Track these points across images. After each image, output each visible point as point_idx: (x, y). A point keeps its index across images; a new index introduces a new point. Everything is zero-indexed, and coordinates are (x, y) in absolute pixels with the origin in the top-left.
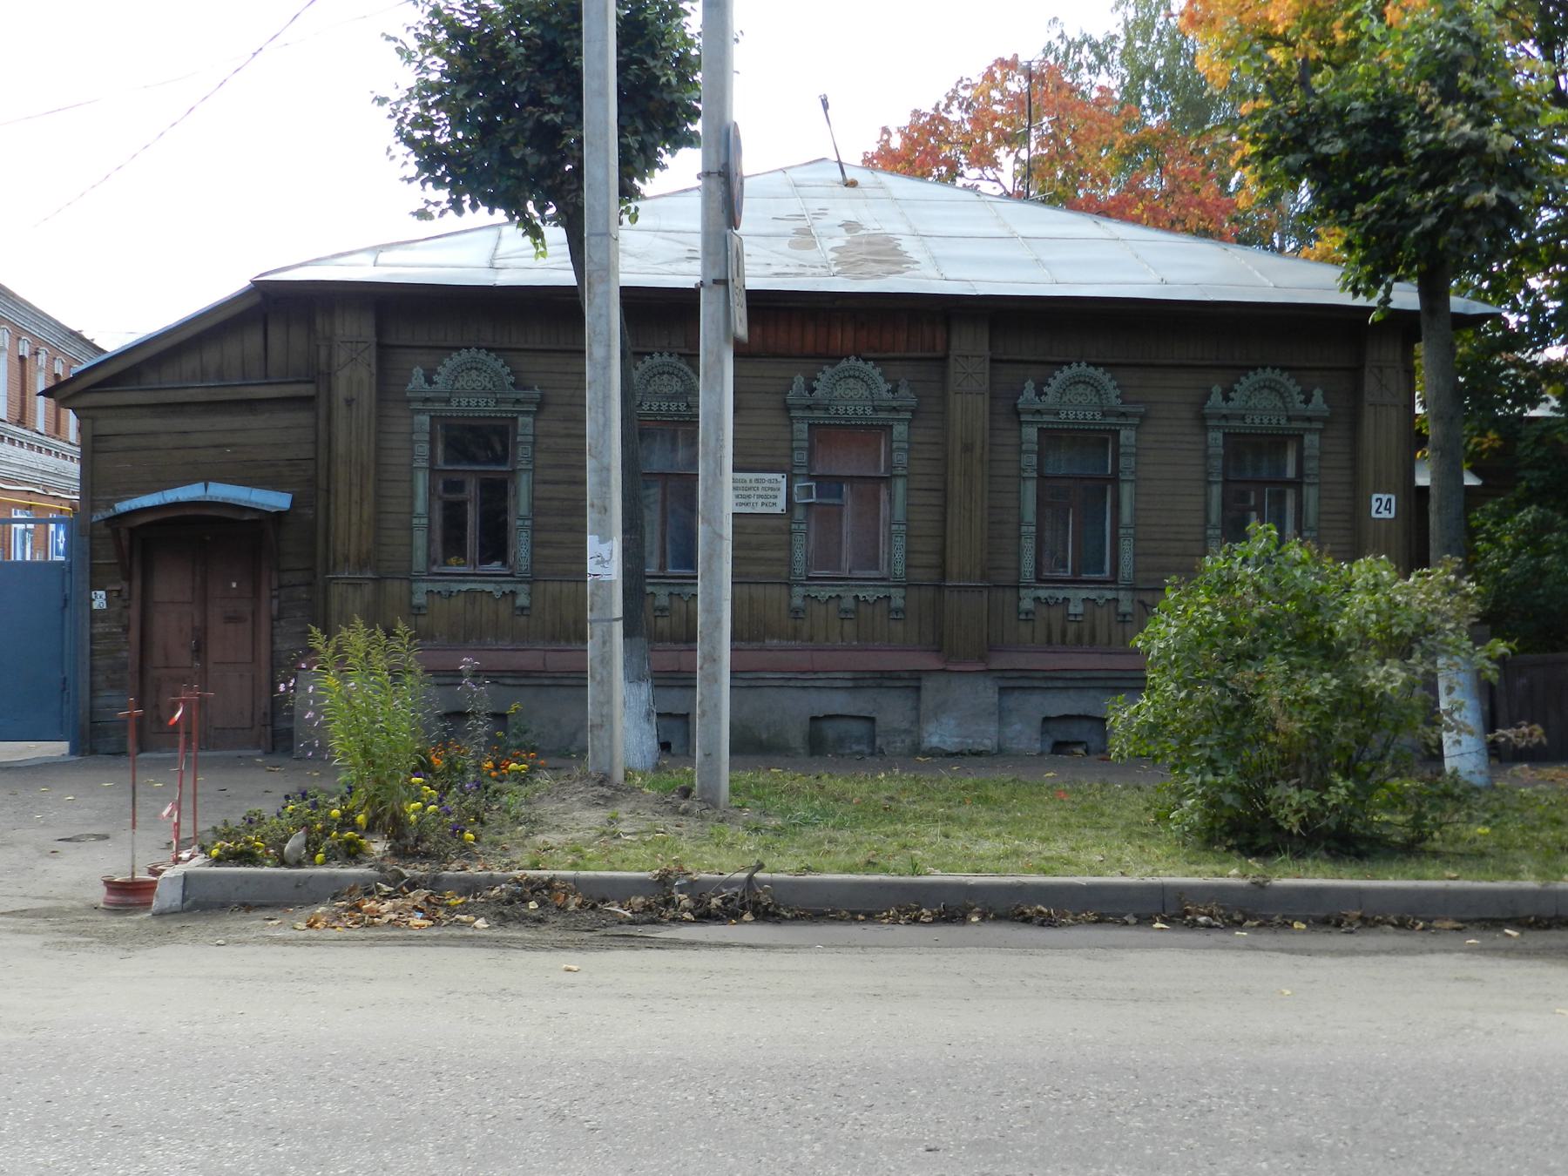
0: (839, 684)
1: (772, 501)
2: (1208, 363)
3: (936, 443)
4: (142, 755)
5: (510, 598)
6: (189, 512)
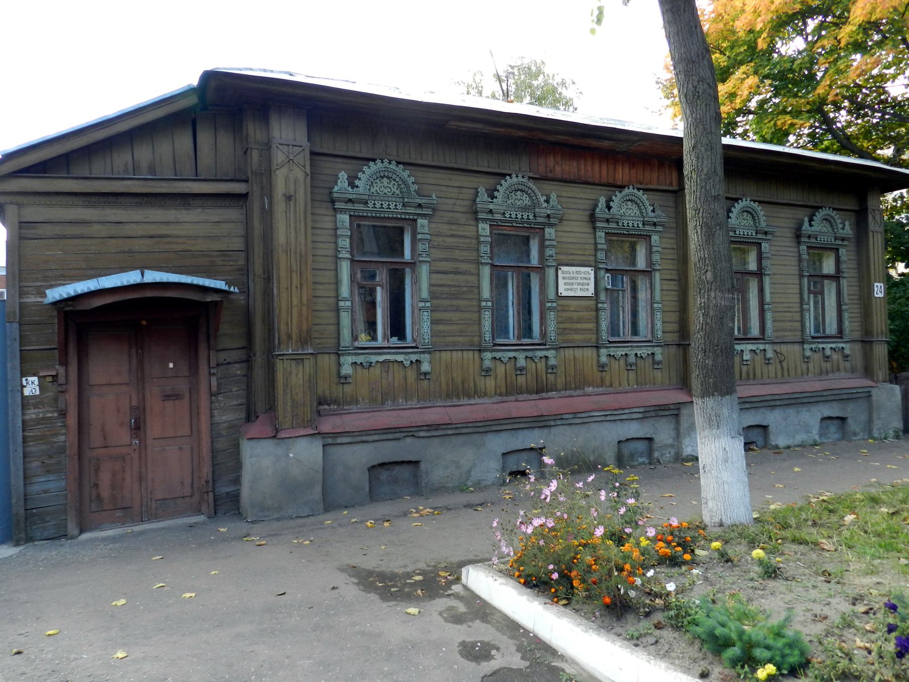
0: (635, 416)
1: (586, 287)
2: (799, 203)
3: (673, 249)
4: (85, 536)
5: (415, 366)
6: (149, 294)
